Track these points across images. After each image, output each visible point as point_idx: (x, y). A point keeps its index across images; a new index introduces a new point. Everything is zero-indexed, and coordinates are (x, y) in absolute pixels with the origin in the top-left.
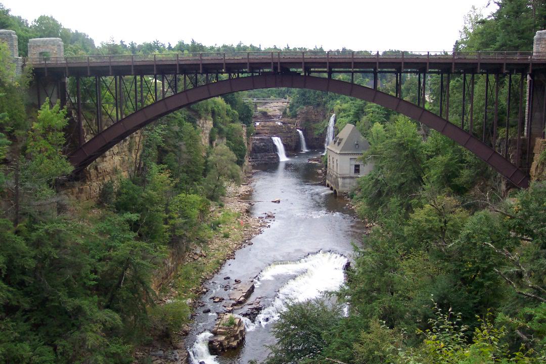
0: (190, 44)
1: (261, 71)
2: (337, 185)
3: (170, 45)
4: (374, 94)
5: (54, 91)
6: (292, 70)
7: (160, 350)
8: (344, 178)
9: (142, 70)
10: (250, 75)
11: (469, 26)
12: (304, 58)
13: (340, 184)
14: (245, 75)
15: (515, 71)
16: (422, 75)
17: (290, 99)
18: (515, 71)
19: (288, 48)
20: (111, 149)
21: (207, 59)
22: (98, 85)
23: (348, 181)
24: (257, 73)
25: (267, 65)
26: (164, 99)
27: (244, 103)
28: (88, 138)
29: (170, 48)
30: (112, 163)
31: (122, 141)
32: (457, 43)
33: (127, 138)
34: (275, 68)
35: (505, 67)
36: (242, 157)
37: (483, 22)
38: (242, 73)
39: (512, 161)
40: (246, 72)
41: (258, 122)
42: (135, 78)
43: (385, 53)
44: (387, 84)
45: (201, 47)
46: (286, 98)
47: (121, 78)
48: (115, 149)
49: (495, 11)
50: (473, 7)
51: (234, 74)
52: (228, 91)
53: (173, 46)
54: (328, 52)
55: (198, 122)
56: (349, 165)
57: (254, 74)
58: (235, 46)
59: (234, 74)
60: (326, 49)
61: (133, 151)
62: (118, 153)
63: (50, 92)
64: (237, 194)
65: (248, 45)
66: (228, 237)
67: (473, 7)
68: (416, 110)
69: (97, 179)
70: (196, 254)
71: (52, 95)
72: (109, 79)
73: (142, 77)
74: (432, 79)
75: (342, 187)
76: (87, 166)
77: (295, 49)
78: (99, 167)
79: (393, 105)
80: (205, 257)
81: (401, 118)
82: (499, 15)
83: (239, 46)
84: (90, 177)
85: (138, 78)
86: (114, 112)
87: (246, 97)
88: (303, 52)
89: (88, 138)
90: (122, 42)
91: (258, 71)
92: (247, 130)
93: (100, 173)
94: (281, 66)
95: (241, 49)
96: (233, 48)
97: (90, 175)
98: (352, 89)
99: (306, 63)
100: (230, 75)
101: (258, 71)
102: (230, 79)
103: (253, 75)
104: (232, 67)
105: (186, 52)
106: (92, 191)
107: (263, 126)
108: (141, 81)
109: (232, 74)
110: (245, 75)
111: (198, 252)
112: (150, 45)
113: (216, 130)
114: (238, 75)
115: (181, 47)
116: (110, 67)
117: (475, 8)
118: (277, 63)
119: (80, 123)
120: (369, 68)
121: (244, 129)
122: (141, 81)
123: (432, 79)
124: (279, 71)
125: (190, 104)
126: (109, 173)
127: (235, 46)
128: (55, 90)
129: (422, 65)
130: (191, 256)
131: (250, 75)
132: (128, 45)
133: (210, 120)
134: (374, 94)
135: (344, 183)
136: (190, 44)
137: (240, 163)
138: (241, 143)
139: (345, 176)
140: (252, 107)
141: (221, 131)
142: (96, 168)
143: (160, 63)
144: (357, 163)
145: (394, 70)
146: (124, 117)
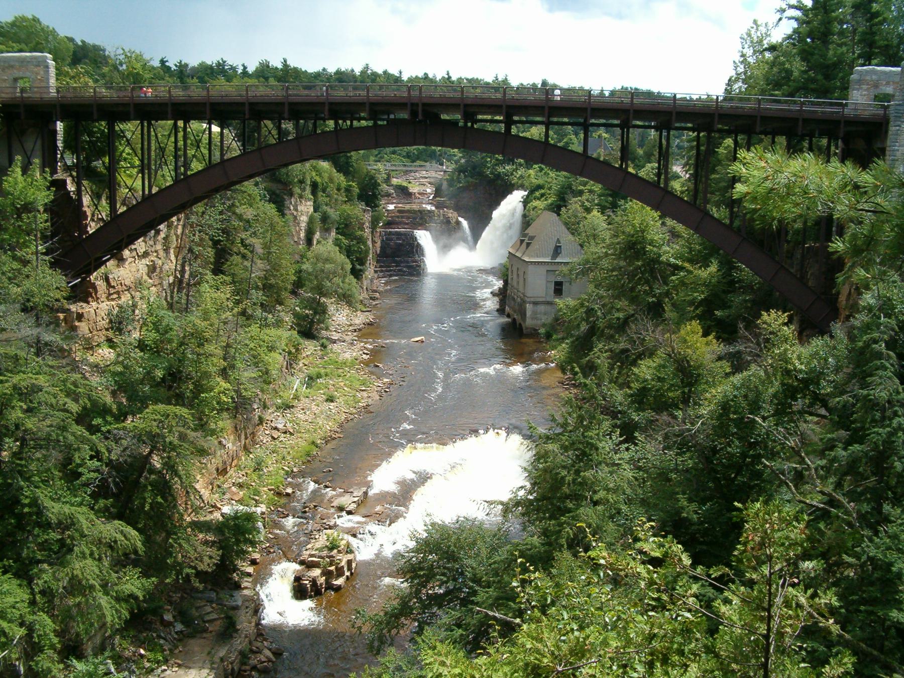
0: (280, 66)
1: (392, 116)
2: (523, 314)
3: (245, 68)
4: (583, 164)
5: (33, 142)
6: (444, 117)
7: (211, 590)
8: (535, 303)
9: (185, 111)
10: (370, 123)
11: (749, 52)
12: (504, 100)
13: (529, 313)
14: (364, 123)
15: (817, 132)
16: (664, 134)
17: (449, 167)
18: (817, 132)
19: (450, 77)
20: (133, 247)
21: (300, 94)
22: (112, 137)
23: (542, 308)
24: (384, 120)
25: (400, 105)
26: (223, 161)
27: (368, 172)
28: (92, 228)
29: (245, 73)
30: (133, 269)
31: (153, 232)
32: (730, 83)
33: (162, 227)
34: (414, 114)
35: (758, 122)
36: (362, 261)
37: (772, 48)
38: (359, 119)
39: (810, 284)
40: (364, 119)
41: (392, 203)
42: (175, 125)
43: (613, 93)
44: (605, 144)
45: (297, 73)
46: (442, 164)
47: (149, 125)
48: (140, 245)
49: (789, 31)
50: (755, 22)
51: (344, 121)
52: (336, 151)
53: (251, 69)
54: (518, 88)
55: (287, 203)
56: (545, 282)
57: (380, 123)
58: (357, 71)
59: (344, 121)
60: (514, 82)
61: (172, 251)
62: (146, 254)
63: (29, 145)
64: (351, 328)
65: (380, 72)
66: (332, 401)
67: (755, 22)
68: (657, 195)
69: (107, 298)
70: (276, 428)
71: (33, 150)
72: (130, 128)
73: (186, 122)
74: (683, 139)
75: (532, 319)
76: (92, 274)
77: (460, 80)
78: (111, 276)
79: (619, 185)
80: (291, 434)
81: (634, 205)
82: (796, 37)
83: (363, 73)
84: (96, 294)
85: (181, 123)
86: (139, 183)
87: (380, 165)
88: (502, 86)
89: (92, 228)
90: (163, 62)
91: (386, 117)
92: (372, 217)
93: (114, 287)
94: (423, 111)
95: (368, 78)
96: (354, 76)
97: (96, 292)
98: (543, 153)
99: (466, 106)
100: (336, 124)
101: (386, 117)
102: (337, 130)
103: (375, 123)
104: (340, 110)
105: (272, 81)
106: (99, 318)
107: (399, 211)
108: (185, 129)
109: (340, 122)
110: (364, 123)
111: (280, 426)
112: (211, 67)
113: (317, 216)
114: (352, 123)
115: (264, 71)
116: (247, 106)
117: (759, 23)
118: (417, 105)
119: (80, 200)
120: (687, 122)
121: (367, 218)
122: (185, 129)
123: (683, 139)
124: (420, 117)
125: (270, 167)
126: (129, 289)
127: (357, 71)
128: (39, 142)
129: (665, 114)
130: (267, 432)
131: (370, 123)
132: (174, 68)
133: (310, 200)
134: (583, 164)
135: (534, 313)
136: (280, 66)
137: (357, 273)
138: (361, 240)
139: (538, 300)
140: (380, 178)
141: (325, 219)
142: (107, 280)
143: (219, 100)
144: (559, 279)
145: (616, 122)
146: (155, 190)
